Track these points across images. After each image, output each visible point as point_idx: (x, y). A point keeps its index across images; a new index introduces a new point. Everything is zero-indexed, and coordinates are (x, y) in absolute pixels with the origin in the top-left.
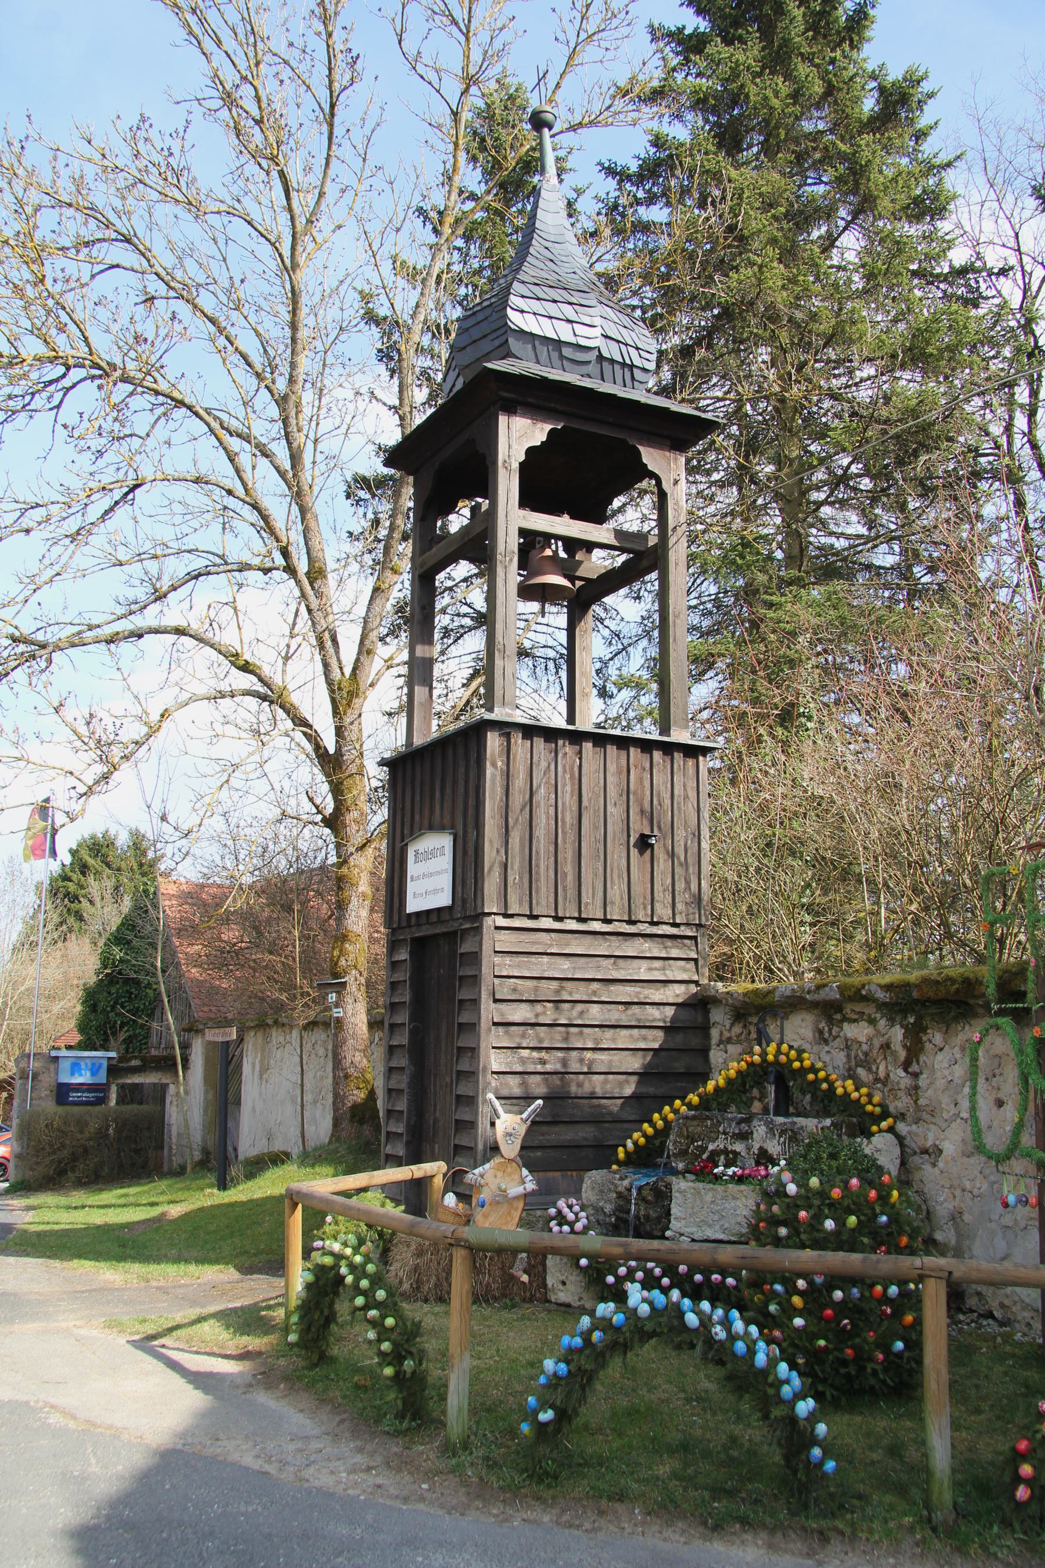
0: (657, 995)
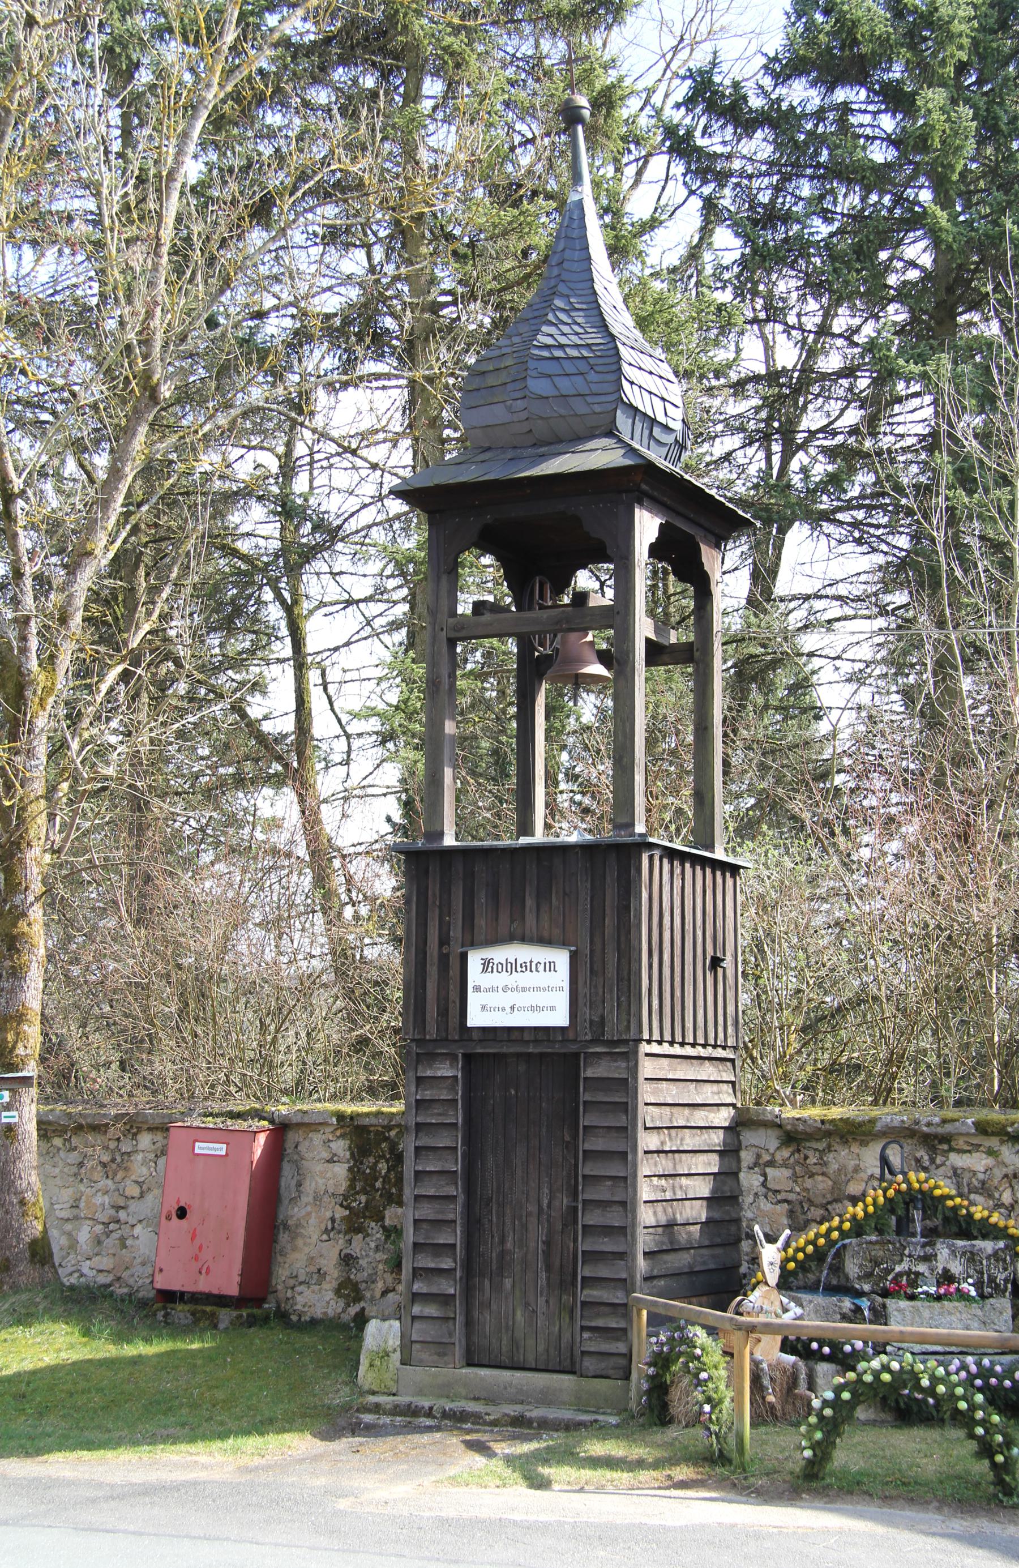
0: (700, 1118)
